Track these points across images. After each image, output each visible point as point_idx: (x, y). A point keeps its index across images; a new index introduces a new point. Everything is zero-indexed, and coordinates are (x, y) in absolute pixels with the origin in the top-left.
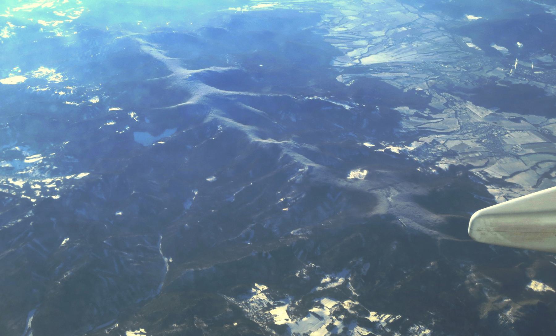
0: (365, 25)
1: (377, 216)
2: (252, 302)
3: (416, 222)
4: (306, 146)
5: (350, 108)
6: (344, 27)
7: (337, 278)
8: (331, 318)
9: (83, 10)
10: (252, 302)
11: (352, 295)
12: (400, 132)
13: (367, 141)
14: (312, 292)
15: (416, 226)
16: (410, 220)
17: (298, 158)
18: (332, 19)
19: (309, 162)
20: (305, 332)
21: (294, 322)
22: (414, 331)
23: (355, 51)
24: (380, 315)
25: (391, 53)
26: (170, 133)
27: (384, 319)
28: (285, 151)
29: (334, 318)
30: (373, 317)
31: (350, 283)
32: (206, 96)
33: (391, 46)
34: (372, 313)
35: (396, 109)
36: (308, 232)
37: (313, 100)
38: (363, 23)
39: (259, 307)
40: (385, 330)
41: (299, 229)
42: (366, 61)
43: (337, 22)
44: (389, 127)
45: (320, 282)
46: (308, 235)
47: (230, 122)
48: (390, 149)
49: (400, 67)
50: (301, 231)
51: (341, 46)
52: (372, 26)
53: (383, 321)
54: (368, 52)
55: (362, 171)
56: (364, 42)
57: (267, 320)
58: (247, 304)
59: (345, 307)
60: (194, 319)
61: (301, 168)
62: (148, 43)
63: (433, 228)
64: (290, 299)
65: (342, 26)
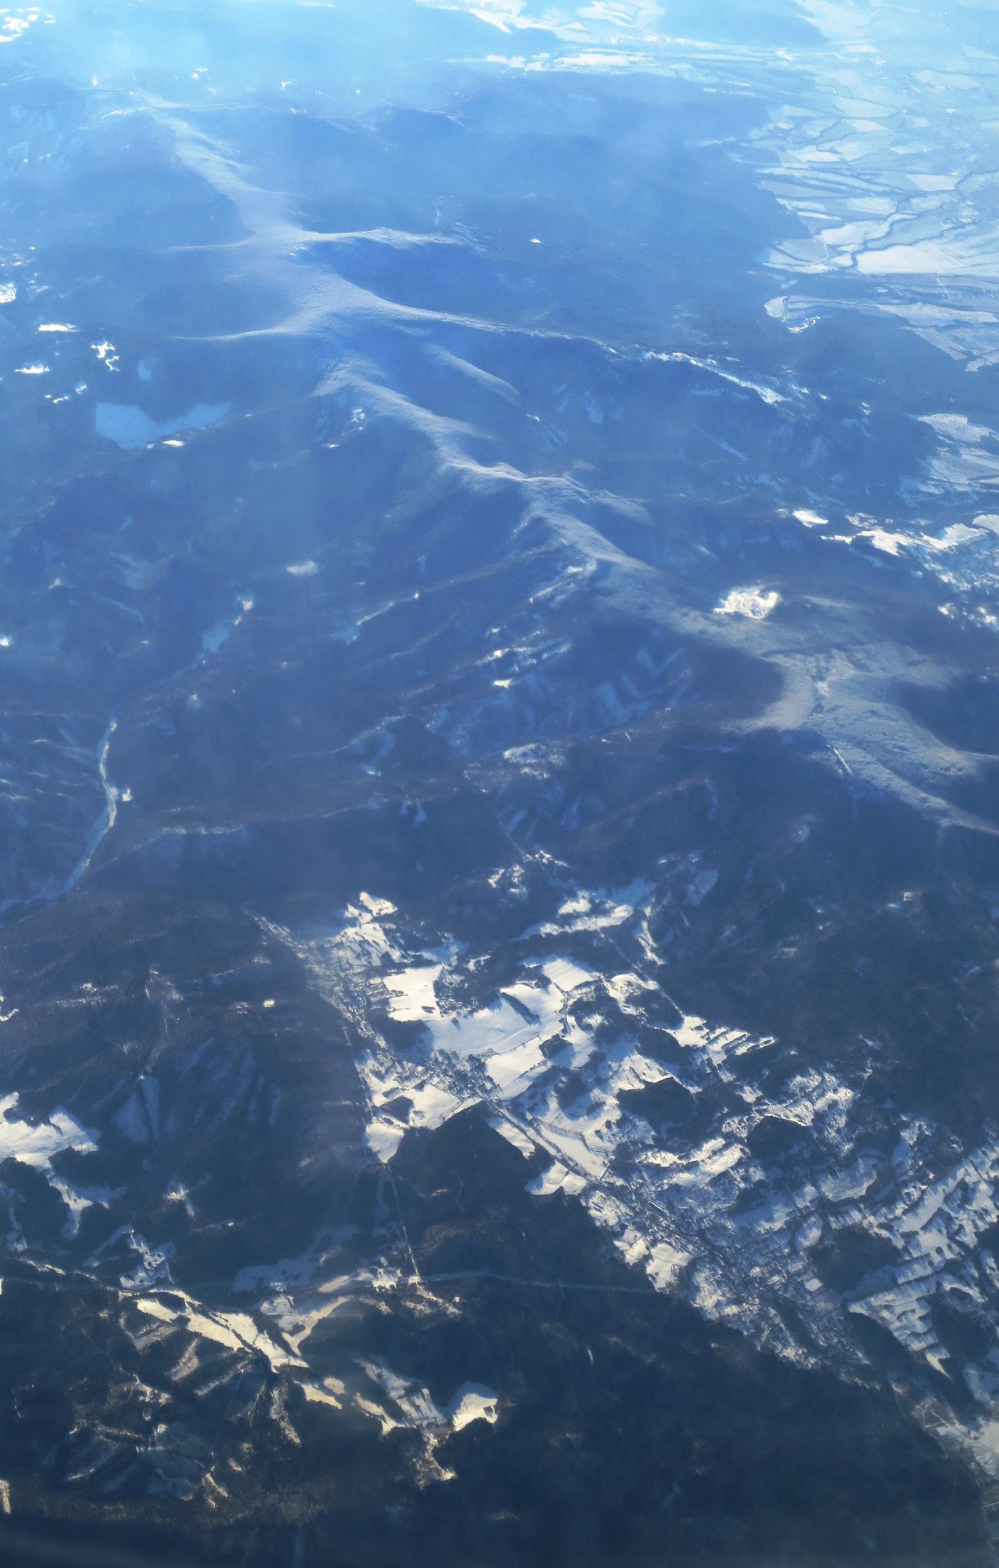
0: (901, 151)
1: (771, 734)
2: (340, 945)
3: (885, 764)
4: (608, 499)
5: (780, 398)
6: (832, 151)
7: (609, 904)
8: (563, 1021)
9: (33, 18)
10: (340, 945)
11: (642, 960)
12: (918, 492)
13: (806, 505)
14: (526, 936)
15: (883, 777)
16: (869, 758)
17: (574, 531)
18: (800, 122)
19: (605, 548)
20: (475, 1053)
21: (448, 1018)
22: (802, 1088)
23: (848, 229)
24: (712, 1030)
25: (958, 247)
26: (207, 416)
27: (722, 1042)
28: (537, 509)
29: (571, 1020)
30: (689, 1033)
31: (645, 925)
32: (336, 315)
33: (963, 225)
34: (691, 1021)
35: (926, 419)
36: (555, 759)
37: (670, 364)
38: (896, 143)
39: (355, 962)
40: (717, 1075)
41: (532, 746)
42: (871, 264)
43: (813, 131)
44: (885, 468)
45: (555, 910)
46: (550, 767)
47: (393, 401)
48: (869, 539)
49: (977, 293)
50: (536, 753)
51: (809, 209)
52: (919, 156)
53: (717, 1047)
54: (888, 234)
55: (763, 594)
56: (881, 205)
57: (369, 1004)
58: (322, 949)
59: (612, 993)
60: (147, 975)
61: (574, 564)
62: (203, 136)
63: (933, 789)
64: (454, 949)
65: (827, 146)
